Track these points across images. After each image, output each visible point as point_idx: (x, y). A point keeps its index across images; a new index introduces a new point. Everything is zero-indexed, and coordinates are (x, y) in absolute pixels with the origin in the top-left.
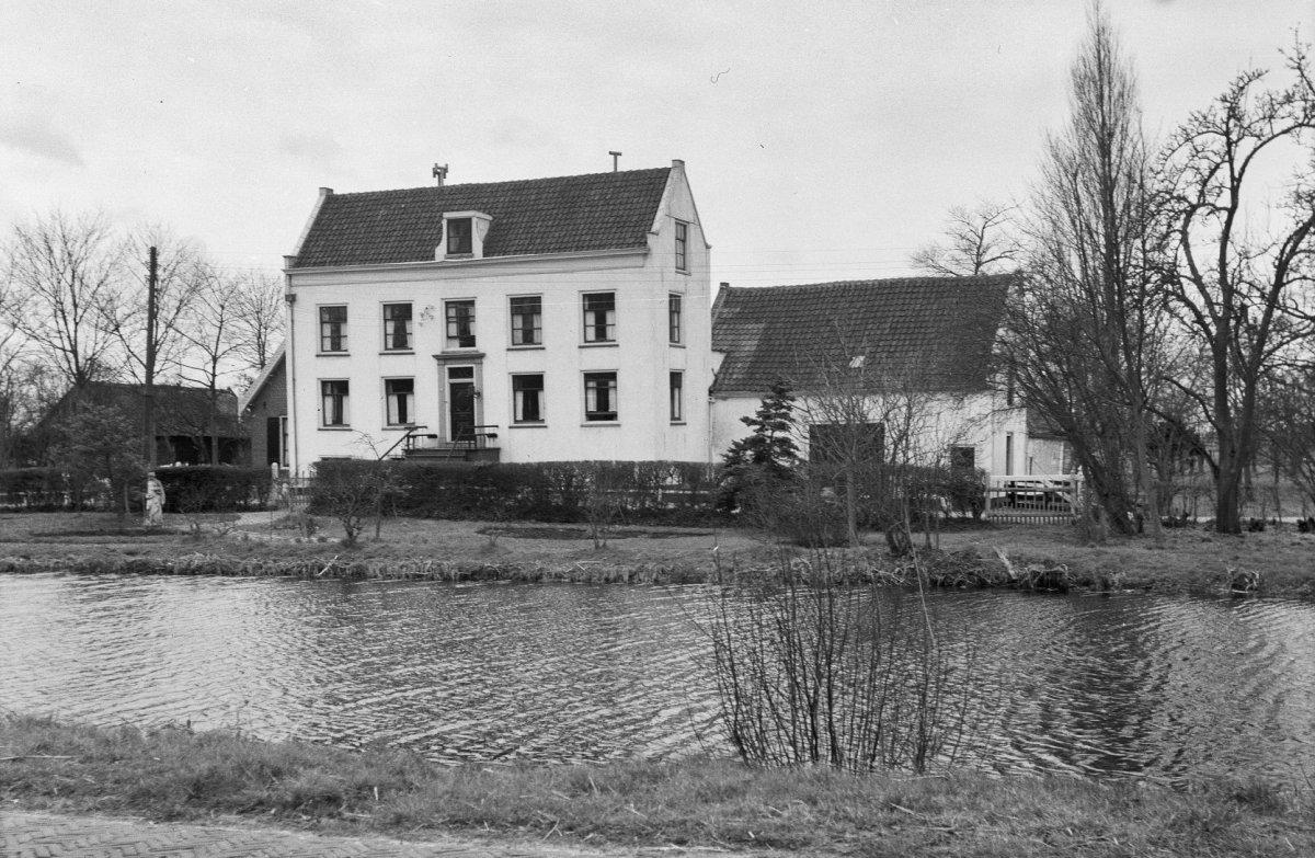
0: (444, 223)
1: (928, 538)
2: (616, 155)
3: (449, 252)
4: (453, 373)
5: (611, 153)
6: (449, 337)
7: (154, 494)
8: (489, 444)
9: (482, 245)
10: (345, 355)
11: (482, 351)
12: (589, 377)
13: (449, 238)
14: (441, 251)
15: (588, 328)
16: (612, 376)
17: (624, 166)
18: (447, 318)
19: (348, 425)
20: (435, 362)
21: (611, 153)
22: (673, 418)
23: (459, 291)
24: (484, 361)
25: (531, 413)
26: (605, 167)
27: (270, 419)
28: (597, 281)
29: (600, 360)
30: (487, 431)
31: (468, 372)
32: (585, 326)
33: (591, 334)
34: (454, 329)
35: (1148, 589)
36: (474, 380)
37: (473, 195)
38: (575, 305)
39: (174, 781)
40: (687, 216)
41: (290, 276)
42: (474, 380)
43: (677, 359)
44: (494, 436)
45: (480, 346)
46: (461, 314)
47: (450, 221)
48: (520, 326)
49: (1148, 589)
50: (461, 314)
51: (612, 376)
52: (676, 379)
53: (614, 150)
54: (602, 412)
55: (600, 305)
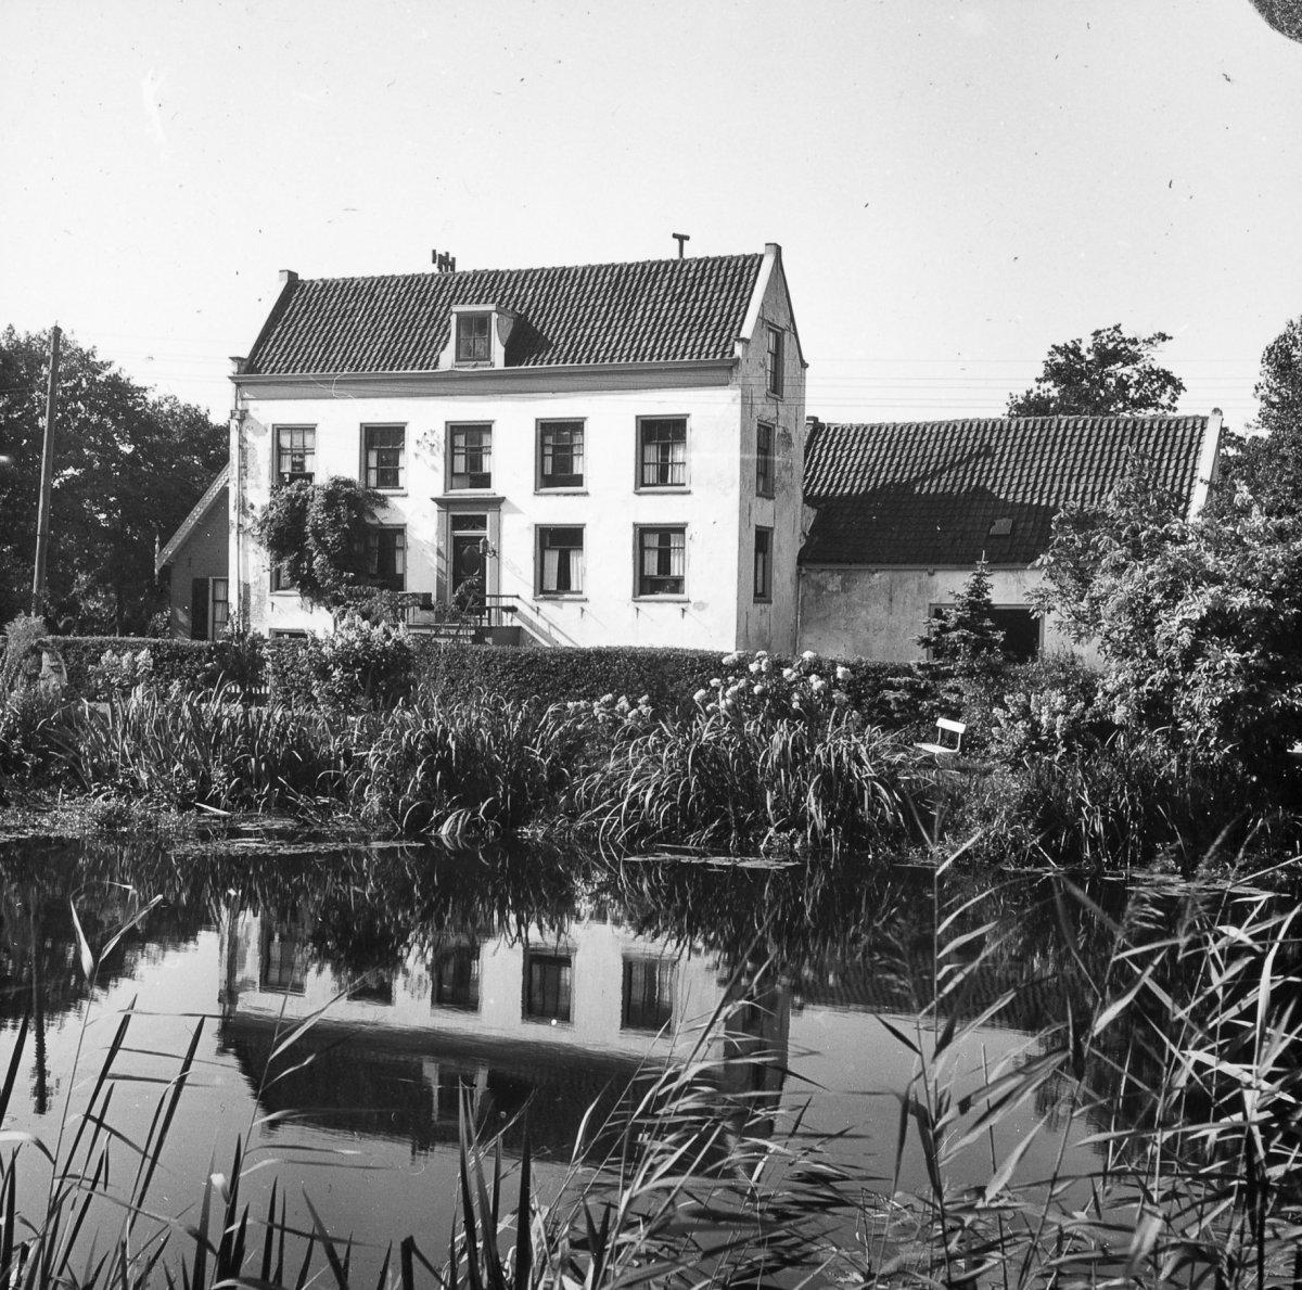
1: (280, 975)
2: (682, 238)
3: (458, 359)
4: (457, 522)
5: (675, 236)
6: (453, 474)
8: (508, 620)
9: (503, 350)
11: (500, 494)
13: (458, 335)
14: (447, 359)
15: (646, 468)
16: (680, 529)
17: (693, 251)
18: (453, 447)
19: (580, 593)
20: (435, 506)
21: (675, 236)
22: (756, 594)
24: (503, 507)
25: (557, 582)
26: (669, 252)
27: (196, 580)
28: (662, 402)
30: (505, 602)
31: (480, 522)
34: (460, 464)
35: (1048, 1055)
36: (487, 533)
37: (489, 283)
42: (487, 533)
45: (497, 488)
46: (468, 443)
47: (461, 317)
49: (1048, 1055)
50: (468, 443)
51: (680, 529)
53: (677, 232)
55: (661, 435)
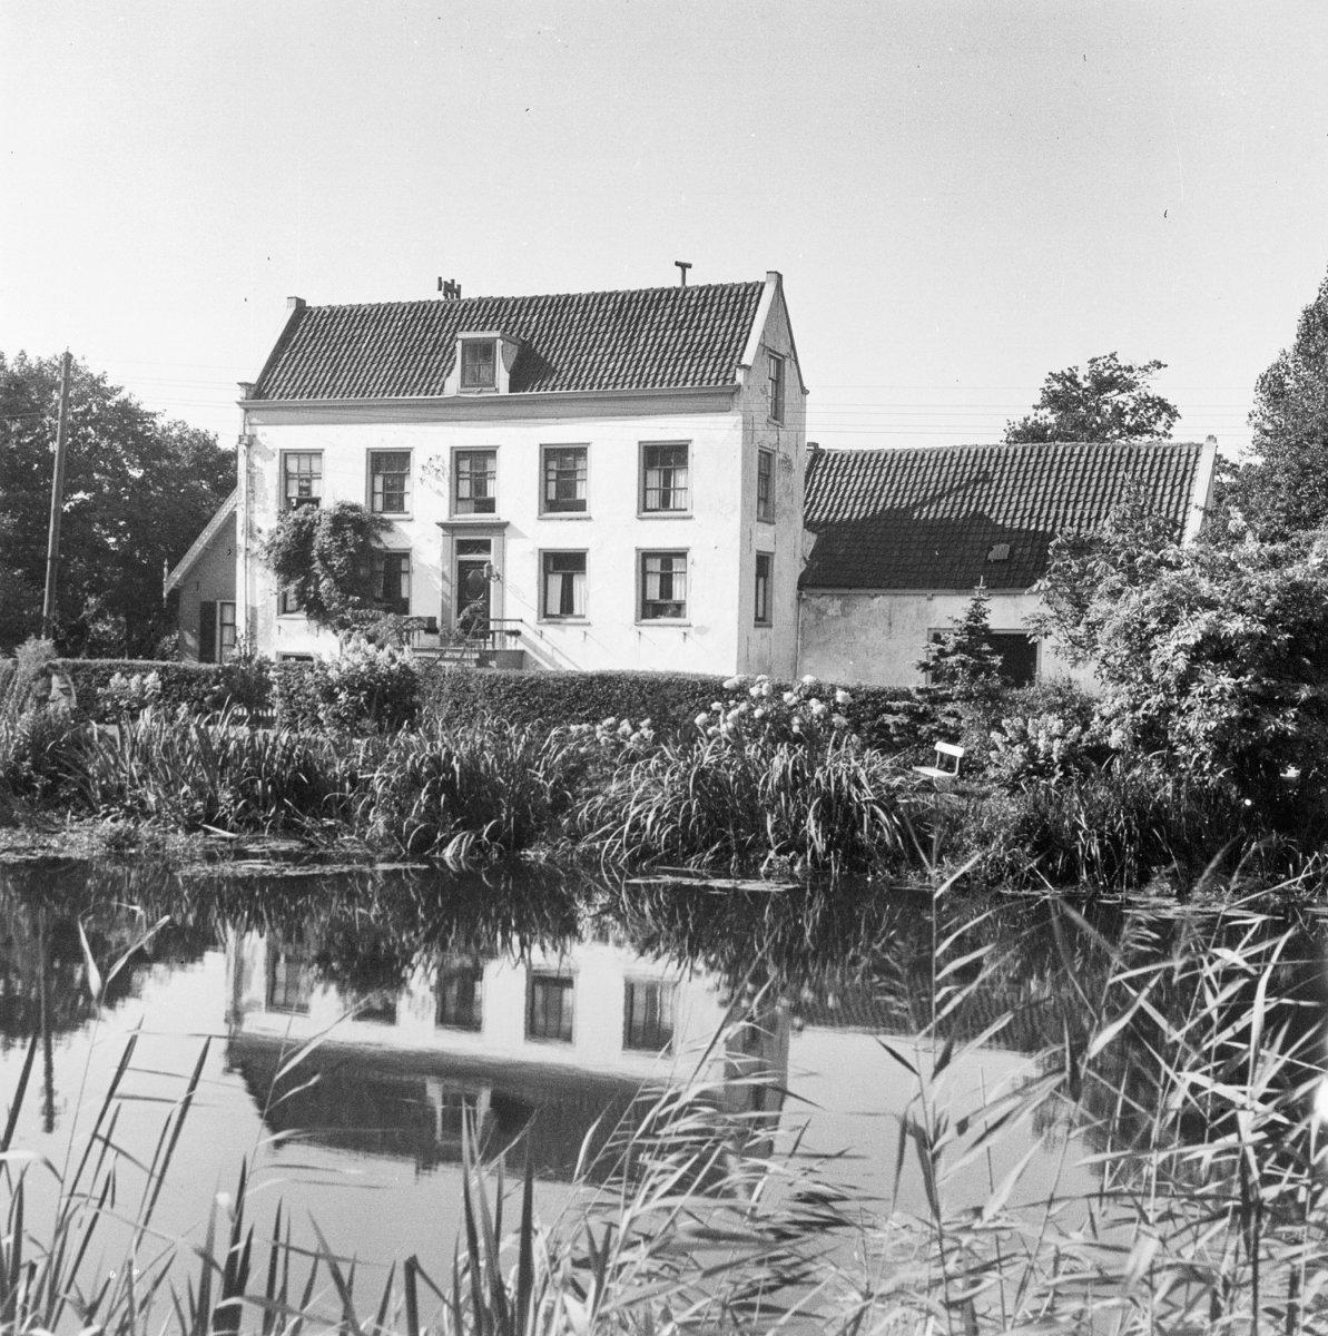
0: (459, 345)
2: (684, 266)
4: (463, 547)
5: (677, 264)
6: (459, 499)
7: (61, 695)
8: (512, 644)
9: (508, 376)
10: (684, 518)
11: (504, 519)
12: (645, 556)
14: (452, 385)
18: (458, 472)
20: (440, 531)
21: (677, 264)
22: (757, 619)
23: (473, 435)
28: (664, 428)
29: (662, 534)
30: (509, 626)
31: (485, 546)
32: (646, 490)
33: (654, 499)
34: (465, 489)
36: (492, 557)
37: (494, 310)
38: (629, 465)
39: (1262, 702)
40: (784, 349)
41: (247, 410)
42: (492, 557)
43: (764, 538)
44: (516, 633)
45: (502, 513)
48: (656, 485)
50: (473, 466)
52: (763, 564)
54: (658, 605)
55: (663, 460)
